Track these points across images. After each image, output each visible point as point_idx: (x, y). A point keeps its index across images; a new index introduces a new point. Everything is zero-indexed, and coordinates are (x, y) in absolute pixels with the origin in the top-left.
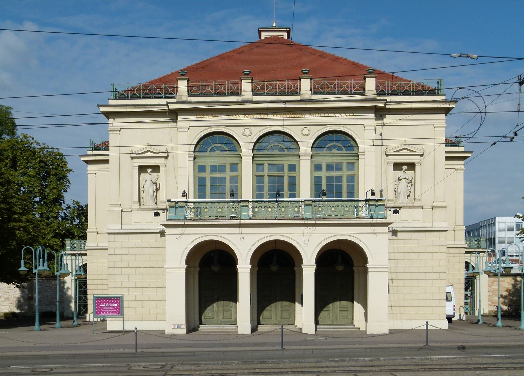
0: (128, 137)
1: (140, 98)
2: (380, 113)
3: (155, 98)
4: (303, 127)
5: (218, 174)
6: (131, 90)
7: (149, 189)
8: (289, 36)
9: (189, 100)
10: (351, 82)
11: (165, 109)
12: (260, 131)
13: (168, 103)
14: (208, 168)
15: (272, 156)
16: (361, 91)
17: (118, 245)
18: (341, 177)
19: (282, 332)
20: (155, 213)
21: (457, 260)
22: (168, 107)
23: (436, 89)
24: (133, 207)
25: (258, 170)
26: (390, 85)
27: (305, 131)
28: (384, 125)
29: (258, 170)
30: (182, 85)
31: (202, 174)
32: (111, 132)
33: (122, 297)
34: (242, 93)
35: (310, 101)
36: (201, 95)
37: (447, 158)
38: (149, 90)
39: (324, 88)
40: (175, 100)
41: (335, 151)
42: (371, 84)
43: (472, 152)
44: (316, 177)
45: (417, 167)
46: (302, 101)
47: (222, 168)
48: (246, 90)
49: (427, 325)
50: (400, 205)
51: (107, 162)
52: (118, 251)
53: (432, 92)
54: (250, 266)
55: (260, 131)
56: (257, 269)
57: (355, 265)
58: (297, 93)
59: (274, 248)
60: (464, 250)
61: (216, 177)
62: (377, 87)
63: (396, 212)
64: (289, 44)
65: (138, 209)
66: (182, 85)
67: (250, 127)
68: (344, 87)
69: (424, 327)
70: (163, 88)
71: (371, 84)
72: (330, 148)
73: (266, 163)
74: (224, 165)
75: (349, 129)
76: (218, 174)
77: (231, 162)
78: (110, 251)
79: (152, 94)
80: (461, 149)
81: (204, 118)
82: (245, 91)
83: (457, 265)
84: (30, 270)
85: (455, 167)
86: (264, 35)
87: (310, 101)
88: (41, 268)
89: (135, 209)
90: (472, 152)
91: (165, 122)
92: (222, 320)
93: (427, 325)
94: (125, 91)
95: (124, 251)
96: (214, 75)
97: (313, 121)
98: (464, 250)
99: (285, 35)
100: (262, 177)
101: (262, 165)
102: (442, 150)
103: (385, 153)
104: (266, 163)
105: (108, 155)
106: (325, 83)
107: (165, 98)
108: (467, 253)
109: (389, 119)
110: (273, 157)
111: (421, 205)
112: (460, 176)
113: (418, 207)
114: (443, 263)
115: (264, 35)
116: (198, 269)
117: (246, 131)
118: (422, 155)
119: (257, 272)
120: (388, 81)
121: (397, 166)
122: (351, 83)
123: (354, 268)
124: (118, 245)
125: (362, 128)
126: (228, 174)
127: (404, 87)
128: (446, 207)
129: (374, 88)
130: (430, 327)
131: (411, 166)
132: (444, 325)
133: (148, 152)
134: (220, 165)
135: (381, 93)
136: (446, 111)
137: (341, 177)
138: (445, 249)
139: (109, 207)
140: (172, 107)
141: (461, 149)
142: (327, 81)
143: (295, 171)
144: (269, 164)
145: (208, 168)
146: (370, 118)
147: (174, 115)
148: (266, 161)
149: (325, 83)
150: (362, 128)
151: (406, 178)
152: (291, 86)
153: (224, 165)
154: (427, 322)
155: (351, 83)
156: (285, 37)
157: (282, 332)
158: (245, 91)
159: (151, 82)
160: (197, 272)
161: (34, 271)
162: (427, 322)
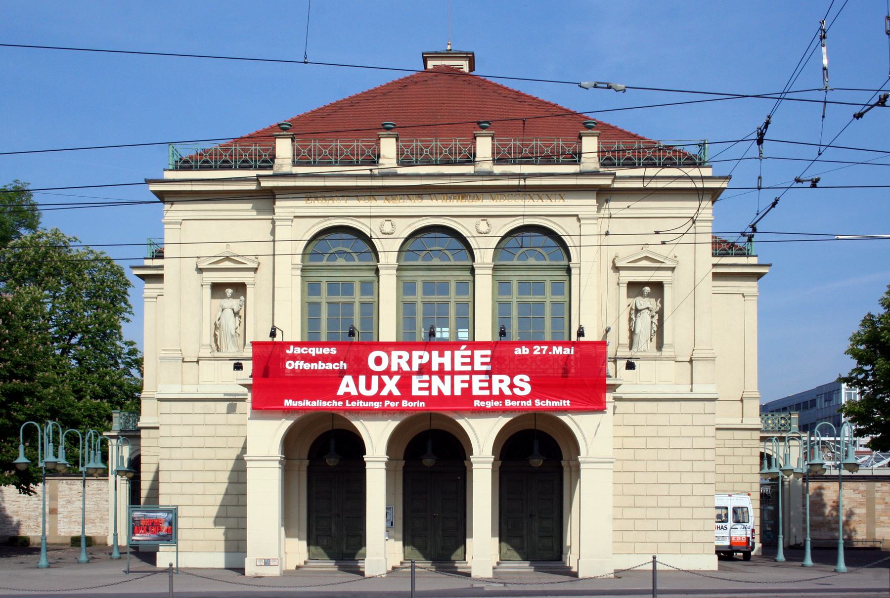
0: (198, 235)
1: (216, 169)
2: (604, 194)
3: (240, 170)
4: (383, 220)
5: (435, 298)
6: (201, 155)
7: (644, 324)
8: (472, 67)
9: (294, 172)
10: (456, 143)
11: (253, 187)
12: (409, 226)
13: (258, 176)
14: (324, 288)
15: (429, 268)
16: (575, 157)
17: (176, 419)
18: (542, 303)
19: (413, 572)
20: (235, 364)
21: (747, 452)
22: (259, 183)
23: (176, 162)
24: (202, 355)
25: (406, 292)
26: (623, 150)
27: (485, 224)
28: (610, 217)
29: (406, 292)
30: (284, 148)
31: (314, 299)
32: (166, 226)
33: (176, 509)
34: (381, 161)
35: (490, 175)
36: (315, 164)
37: (716, 276)
38: (614, 151)
39: (315, 155)
40: (270, 172)
41: (341, 262)
42: (590, 145)
43: (770, 265)
44: (310, 304)
45: (249, 290)
46: (383, 176)
47: (347, 288)
48: (386, 155)
49: (654, 562)
50: (638, 355)
51: (159, 278)
52: (176, 431)
53: (692, 162)
54: (385, 458)
55: (409, 226)
56: (500, 463)
57: (564, 458)
58: (310, 163)
59: (330, 428)
60: (758, 435)
61: (337, 303)
62: (400, 152)
63: (630, 366)
64: (469, 79)
65: (209, 359)
66: (284, 148)
67: (393, 220)
68: (548, 151)
69: (650, 567)
70: (254, 151)
71: (590, 145)
72: (333, 256)
73: (324, 280)
74: (351, 284)
75: (555, 223)
76: (435, 298)
77: (424, 279)
78: (162, 431)
79: (236, 162)
80: (753, 260)
81: (426, 202)
82: (384, 157)
83: (747, 460)
84: (34, 460)
85: (742, 290)
86: (431, 64)
87: (396, 176)
88: (50, 458)
89: (205, 358)
90: (770, 265)
91: (245, 208)
92: (345, 551)
93: (654, 562)
94: (191, 157)
95: (187, 431)
96: (337, 131)
97: (449, 209)
98: (758, 435)
99: (465, 66)
100: (413, 304)
101: (413, 283)
102: (706, 258)
103: (613, 262)
104: (324, 280)
105: (162, 267)
106: (315, 146)
107: (256, 168)
108: (763, 439)
109: (616, 206)
110: (430, 270)
111: (673, 354)
112: (752, 306)
113: (668, 358)
114: (710, 455)
115: (431, 64)
116: (306, 463)
117: (390, 224)
118: (255, 270)
119: (404, 467)
120: (619, 143)
121: (218, 289)
122: (558, 144)
123: (564, 463)
124: (176, 419)
125: (577, 220)
126: (357, 297)
127: (241, 155)
128: (713, 359)
129: (394, 154)
130: (659, 567)
131: (240, 288)
132: (712, 563)
133: (227, 258)
134: (344, 283)
135: (689, 162)
136: (714, 194)
137: (542, 303)
138: (711, 431)
139: (162, 354)
140: (265, 184)
141: (753, 260)
142: (421, 141)
143: (362, 295)
144: (425, 283)
145: (324, 288)
146: (586, 205)
147: (265, 198)
148: (420, 277)
149: (315, 146)
150: (577, 220)
151: (648, 308)
152: (441, 149)
153: (351, 284)
154: (654, 558)
155: (558, 144)
156: (466, 69)
157: (413, 572)
158: (384, 157)
159: (236, 140)
160: (305, 469)
161: (41, 465)
162: (654, 558)
